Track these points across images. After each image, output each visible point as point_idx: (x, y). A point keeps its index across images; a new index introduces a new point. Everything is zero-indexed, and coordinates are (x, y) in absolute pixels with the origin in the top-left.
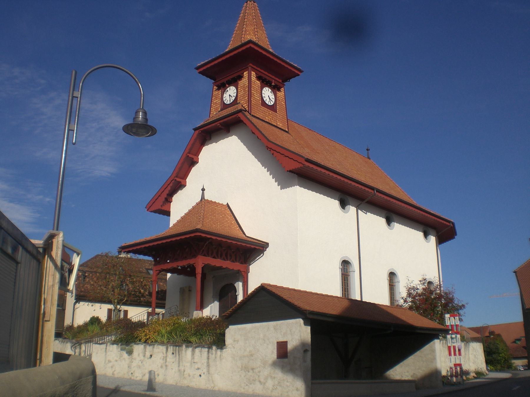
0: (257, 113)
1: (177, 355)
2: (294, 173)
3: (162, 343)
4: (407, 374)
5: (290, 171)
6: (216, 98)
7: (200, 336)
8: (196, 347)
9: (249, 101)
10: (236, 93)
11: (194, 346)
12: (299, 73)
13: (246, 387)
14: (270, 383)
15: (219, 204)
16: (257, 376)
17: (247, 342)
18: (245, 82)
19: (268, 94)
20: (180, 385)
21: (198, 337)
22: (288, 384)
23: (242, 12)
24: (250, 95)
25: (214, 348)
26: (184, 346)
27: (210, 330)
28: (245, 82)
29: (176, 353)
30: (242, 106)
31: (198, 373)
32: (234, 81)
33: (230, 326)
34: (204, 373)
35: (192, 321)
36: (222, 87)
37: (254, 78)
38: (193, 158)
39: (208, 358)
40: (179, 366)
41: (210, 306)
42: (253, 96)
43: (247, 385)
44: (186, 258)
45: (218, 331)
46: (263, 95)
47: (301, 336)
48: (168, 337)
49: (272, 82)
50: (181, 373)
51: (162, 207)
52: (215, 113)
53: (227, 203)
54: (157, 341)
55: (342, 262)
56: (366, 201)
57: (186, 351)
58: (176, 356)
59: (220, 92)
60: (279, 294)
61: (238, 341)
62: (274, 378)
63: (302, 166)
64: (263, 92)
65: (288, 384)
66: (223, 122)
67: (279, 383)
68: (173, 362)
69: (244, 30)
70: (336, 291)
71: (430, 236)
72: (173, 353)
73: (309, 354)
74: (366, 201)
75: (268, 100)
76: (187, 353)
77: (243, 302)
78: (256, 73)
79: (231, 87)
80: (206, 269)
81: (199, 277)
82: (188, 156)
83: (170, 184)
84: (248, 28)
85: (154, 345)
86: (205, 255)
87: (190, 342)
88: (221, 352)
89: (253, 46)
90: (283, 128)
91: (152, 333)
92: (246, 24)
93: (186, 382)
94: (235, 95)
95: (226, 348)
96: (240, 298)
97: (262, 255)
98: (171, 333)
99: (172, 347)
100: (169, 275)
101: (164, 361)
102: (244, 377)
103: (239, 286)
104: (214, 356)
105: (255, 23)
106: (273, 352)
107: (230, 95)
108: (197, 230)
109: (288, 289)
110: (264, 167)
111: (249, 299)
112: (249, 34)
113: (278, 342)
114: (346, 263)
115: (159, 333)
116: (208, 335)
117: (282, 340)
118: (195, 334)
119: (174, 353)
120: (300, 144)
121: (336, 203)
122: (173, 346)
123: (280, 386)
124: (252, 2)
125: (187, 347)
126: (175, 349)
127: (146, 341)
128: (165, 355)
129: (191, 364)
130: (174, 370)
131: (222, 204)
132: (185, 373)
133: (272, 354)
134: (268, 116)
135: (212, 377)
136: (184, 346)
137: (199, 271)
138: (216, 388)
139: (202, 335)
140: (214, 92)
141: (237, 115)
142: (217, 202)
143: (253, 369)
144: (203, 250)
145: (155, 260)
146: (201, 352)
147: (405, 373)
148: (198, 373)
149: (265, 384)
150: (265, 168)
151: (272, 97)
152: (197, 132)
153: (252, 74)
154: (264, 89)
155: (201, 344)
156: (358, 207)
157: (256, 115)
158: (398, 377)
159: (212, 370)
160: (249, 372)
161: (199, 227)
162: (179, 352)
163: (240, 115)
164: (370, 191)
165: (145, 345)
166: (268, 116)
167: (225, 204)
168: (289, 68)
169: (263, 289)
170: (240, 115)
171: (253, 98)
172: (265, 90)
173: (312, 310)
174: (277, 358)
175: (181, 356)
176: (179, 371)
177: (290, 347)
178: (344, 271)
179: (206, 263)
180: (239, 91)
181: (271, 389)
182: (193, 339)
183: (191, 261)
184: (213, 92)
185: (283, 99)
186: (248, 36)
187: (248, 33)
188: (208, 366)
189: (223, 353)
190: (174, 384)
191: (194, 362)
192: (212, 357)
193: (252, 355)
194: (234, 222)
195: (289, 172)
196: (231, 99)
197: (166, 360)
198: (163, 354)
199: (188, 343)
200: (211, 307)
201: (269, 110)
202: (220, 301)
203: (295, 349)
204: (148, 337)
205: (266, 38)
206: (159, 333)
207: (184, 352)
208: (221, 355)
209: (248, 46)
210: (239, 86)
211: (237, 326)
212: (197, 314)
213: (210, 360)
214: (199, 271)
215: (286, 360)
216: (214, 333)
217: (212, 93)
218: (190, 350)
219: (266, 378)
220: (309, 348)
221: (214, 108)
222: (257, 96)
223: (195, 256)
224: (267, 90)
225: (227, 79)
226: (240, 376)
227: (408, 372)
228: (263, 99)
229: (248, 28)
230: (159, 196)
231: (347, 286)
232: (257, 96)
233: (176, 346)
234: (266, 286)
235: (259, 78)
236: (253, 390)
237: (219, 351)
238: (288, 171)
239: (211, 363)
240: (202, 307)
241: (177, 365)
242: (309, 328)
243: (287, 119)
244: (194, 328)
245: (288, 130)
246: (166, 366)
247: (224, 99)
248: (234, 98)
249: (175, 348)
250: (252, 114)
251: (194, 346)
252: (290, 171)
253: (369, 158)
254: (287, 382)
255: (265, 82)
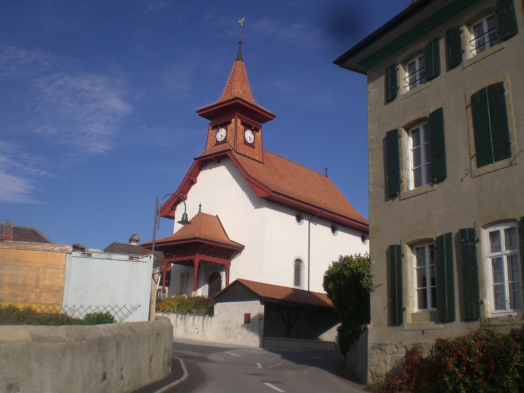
0: (241, 151)
1: (184, 320)
2: (266, 199)
3: (174, 312)
4: (331, 338)
5: (261, 198)
6: (211, 136)
7: (198, 309)
8: (196, 315)
9: (235, 142)
10: (226, 134)
11: (195, 314)
12: (273, 118)
13: (226, 340)
14: (240, 338)
15: (211, 215)
16: (232, 334)
17: (227, 313)
18: (233, 126)
19: (249, 135)
20: (185, 338)
21: (196, 309)
22: (250, 338)
23: (233, 69)
24: (236, 137)
25: (207, 316)
26: (188, 314)
27: (204, 305)
28: (233, 126)
29: (183, 318)
30: (230, 144)
31: (197, 331)
32: (225, 125)
33: (217, 303)
34: (200, 331)
35: (191, 299)
36: (216, 127)
37: (239, 124)
38: (193, 180)
39: (203, 322)
40: (184, 327)
41: (202, 287)
42: (238, 138)
43: (226, 339)
44: (187, 255)
45: (209, 306)
46: (246, 136)
47: (258, 311)
48: (177, 308)
49: (253, 127)
50: (186, 331)
51: (169, 214)
52: (210, 149)
53: (217, 215)
54: (170, 311)
55: (296, 260)
56: (317, 216)
57: (189, 317)
58: (183, 320)
59: (214, 131)
60: (247, 285)
61: (222, 312)
62: (242, 334)
63: (269, 195)
64: (246, 134)
65: (250, 338)
66: (216, 156)
67: (245, 337)
68: (181, 324)
69: (233, 84)
70: (289, 283)
71: (367, 240)
72: (181, 319)
73: (263, 321)
74: (317, 216)
75: (249, 139)
76: (190, 319)
77: (226, 290)
78: (241, 120)
79: (223, 129)
80: (202, 262)
81: (196, 268)
82: (190, 178)
83: (175, 198)
84: (237, 83)
85: (169, 313)
86: (200, 254)
87: (192, 312)
88: (211, 318)
89: (239, 101)
90: (259, 160)
91: (167, 305)
92: (235, 79)
93: (188, 337)
94: (225, 135)
95: (214, 316)
96: (224, 286)
97: (240, 254)
98: (180, 306)
99: (180, 315)
100: (172, 264)
101: (175, 323)
102: (225, 334)
103: (223, 274)
104: (207, 321)
105: (242, 80)
106: (242, 320)
107: (221, 135)
108: (196, 238)
109: (253, 282)
110: (243, 191)
111: (230, 287)
112: (237, 88)
113: (245, 314)
114: (298, 261)
115: (172, 306)
116: (203, 308)
117: (247, 312)
118: (195, 307)
119: (182, 319)
120: (271, 173)
121: (294, 218)
122: (181, 314)
123: (245, 339)
124: (240, 61)
125: (190, 315)
126: (182, 316)
127: (163, 310)
128: (176, 320)
129: (192, 325)
130: (181, 329)
131: (213, 216)
132: (189, 331)
133: (241, 320)
134: (248, 151)
135: (205, 333)
136: (188, 314)
137: (196, 264)
138: (208, 341)
139: (199, 308)
140: (209, 131)
141: (226, 152)
142: (210, 214)
143: (230, 329)
144: (199, 251)
145: (165, 254)
146: (199, 318)
147: (330, 337)
148: (197, 331)
149: (236, 338)
150: (244, 192)
151: (252, 137)
152: (196, 161)
153: (238, 121)
154: (247, 131)
155: (199, 314)
156: (310, 221)
157: (239, 152)
158: (326, 340)
159: (205, 329)
160: (227, 331)
161: (197, 236)
162: (185, 318)
163: (228, 153)
164: (318, 210)
165: (163, 313)
166: (248, 151)
167: (215, 215)
168: (266, 115)
169: (237, 282)
170: (228, 153)
171: (238, 139)
172: (247, 132)
173: (265, 296)
174: (244, 323)
175: (186, 320)
176: (185, 329)
177: (252, 316)
178: (297, 267)
179: (201, 259)
180: (228, 133)
181: (240, 341)
182: (194, 310)
183: (191, 258)
184: (209, 130)
185: (260, 138)
186: (236, 90)
187: (236, 87)
188: (203, 327)
189: (212, 319)
190: (181, 337)
191: (194, 325)
192: (205, 321)
193: (230, 321)
194: (221, 229)
195: (260, 198)
196: (222, 139)
197: (176, 322)
198: (175, 319)
199: (191, 313)
200: (203, 288)
201: (249, 147)
202: (209, 284)
203: (255, 318)
204: (164, 308)
205: (250, 90)
206: (172, 306)
207: (188, 318)
208: (211, 321)
209: (236, 101)
210: (228, 129)
211: (221, 303)
212: (194, 294)
213: (204, 323)
214: (196, 264)
215: (249, 324)
216: (207, 307)
217: (209, 131)
218: (192, 316)
219: (237, 335)
220: (263, 318)
221: (209, 143)
222: (241, 137)
223: (194, 254)
224: (249, 132)
225: (220, 122)
226: (222, 333)
227: (332, 337)
228: (245, 139)
229: (237, 83)
230: (167, 206)
231: (299, 277)
232: (241, 137)
233: (183, 314)
234: (239, 281)
235: (243, 124)
236: (230, 342)
237: (210, 318)
238: (259, 198)
239: (205, 325)
240: (196, 289)
241: (184, 326)
242: (263, 306)
243: (262, 150)
244: (194, 303)
245: (263, 161)
246: (177, 326)
247: (217, 137)
248: (224, 138)
249: (182, 315)
250: (237, 151)
251: (195, 314)
252: (261, 198)
253: (326, 176)
254: (249, 337)
255: (247, 126)
